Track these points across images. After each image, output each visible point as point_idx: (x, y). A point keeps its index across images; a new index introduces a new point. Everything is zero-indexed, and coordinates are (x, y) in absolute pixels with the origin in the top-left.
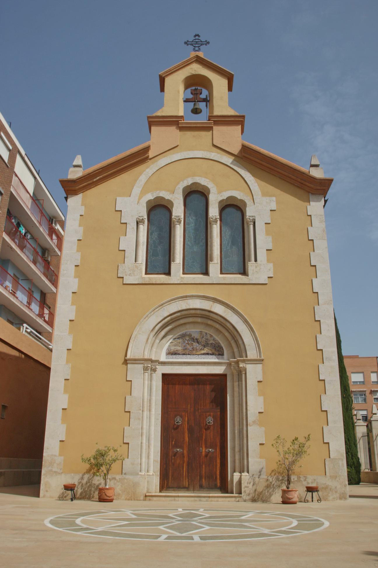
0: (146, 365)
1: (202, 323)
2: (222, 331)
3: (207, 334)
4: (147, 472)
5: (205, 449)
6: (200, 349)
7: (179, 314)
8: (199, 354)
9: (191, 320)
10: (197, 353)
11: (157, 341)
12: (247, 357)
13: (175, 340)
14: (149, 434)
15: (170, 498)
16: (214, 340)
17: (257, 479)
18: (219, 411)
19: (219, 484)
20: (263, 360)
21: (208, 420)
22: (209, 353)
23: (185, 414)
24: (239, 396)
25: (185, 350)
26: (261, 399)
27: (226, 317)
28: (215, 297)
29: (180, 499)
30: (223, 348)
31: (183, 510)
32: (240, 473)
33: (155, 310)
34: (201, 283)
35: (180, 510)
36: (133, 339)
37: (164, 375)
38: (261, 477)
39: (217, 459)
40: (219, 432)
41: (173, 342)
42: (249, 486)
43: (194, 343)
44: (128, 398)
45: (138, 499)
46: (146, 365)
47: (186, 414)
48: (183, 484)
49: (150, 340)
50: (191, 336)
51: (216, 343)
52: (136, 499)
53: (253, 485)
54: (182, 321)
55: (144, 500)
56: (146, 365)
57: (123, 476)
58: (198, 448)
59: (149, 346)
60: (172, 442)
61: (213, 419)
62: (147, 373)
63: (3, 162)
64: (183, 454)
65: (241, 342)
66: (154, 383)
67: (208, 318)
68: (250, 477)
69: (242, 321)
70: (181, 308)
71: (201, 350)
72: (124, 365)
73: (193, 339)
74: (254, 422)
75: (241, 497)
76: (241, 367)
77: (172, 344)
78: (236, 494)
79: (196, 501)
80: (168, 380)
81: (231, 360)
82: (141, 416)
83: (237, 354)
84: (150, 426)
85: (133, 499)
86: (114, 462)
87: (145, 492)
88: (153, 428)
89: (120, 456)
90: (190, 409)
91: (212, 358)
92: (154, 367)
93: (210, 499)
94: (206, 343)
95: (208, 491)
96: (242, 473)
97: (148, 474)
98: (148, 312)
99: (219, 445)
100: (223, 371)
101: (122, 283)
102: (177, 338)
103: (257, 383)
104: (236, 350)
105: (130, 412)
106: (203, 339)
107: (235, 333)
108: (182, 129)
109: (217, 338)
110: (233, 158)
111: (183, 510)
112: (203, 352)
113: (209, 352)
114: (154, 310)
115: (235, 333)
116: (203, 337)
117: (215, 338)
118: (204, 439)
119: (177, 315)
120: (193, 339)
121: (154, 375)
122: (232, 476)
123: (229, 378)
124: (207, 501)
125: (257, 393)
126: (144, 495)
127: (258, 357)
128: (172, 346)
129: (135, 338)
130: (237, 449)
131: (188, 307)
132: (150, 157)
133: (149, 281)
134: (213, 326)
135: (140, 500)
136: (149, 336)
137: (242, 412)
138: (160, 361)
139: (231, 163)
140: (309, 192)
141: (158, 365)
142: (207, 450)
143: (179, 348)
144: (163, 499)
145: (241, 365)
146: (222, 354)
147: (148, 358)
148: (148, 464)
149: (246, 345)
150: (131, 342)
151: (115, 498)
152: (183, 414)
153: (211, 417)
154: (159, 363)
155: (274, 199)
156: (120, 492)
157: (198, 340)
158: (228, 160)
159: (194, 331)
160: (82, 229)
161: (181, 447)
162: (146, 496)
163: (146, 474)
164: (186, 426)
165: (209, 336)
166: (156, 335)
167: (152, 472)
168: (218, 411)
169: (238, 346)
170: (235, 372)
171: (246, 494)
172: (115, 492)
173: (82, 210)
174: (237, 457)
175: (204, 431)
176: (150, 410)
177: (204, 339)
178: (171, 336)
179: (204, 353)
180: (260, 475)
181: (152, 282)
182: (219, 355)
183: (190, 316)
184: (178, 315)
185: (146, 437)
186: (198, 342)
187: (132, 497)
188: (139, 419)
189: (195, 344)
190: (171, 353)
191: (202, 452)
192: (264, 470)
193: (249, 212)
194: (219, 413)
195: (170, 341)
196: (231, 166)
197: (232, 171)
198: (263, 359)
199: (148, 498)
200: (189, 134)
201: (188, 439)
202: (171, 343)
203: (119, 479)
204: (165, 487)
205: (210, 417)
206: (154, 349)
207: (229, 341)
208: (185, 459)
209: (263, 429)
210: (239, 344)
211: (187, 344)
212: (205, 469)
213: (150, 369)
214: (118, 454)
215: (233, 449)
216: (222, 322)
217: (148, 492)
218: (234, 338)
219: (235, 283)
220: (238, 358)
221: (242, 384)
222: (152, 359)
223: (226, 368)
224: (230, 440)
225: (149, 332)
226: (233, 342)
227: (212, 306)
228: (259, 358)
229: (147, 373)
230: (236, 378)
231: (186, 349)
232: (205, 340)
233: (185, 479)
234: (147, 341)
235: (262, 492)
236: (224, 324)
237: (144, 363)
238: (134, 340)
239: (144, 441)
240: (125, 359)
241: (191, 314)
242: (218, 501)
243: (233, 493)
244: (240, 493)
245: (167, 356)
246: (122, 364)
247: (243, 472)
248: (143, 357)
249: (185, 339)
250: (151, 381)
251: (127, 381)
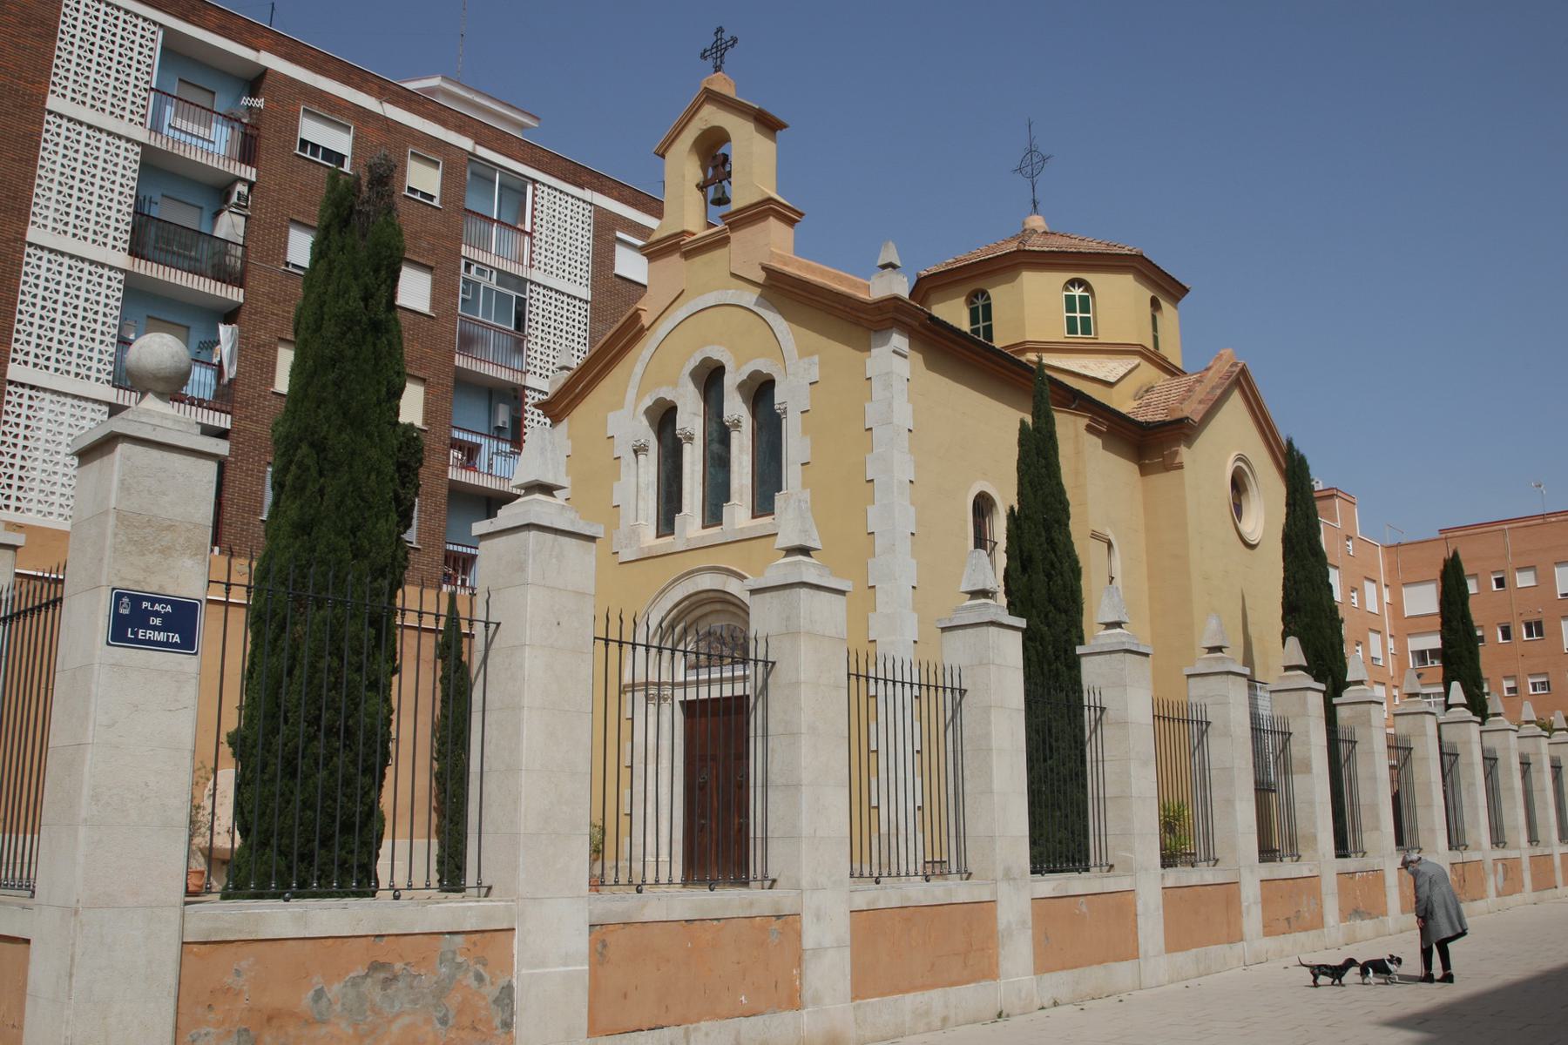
7: (686, 603)
9: (708, 608)
63: (636, 287)
108: (688, 255)
110: (759, 290)
131: (696, 590)
132: (646, 326)
140: (870, 329)
158: (749, 297)
196: (756, 309)
200: (699, 260)
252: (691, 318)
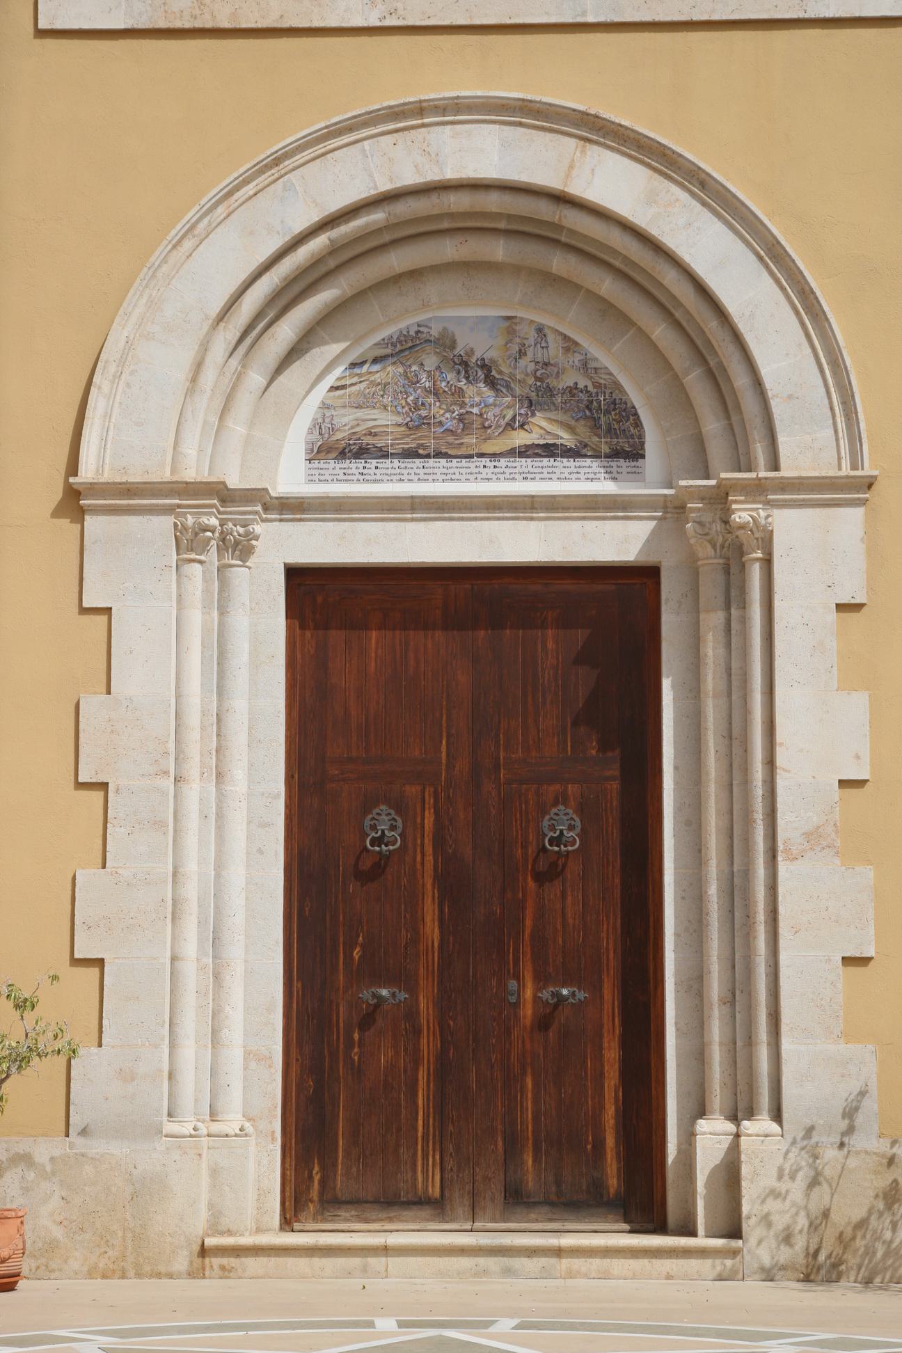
0: (190, 520)
1: (516, 270)
2: (634, 317)
3: (547, 331)
4: (208, 1118)
5: (538, 989)
6: (503, 423)
7: (377, 217)
8: (497, 450)
9: (449, 249)
10: (489, 448)
11: (256, 379)
12: (775, 466)
13: (357, 371)
14: (217, 907)
15: (340, 1262)
17: (831, 1154)
18: (617, 773)
19: (613, 1182)
20: (869, 484)
21: (553, 828)
22: (554, 445)
23: (424, 789)
24: (730, 694)
25: (417, 427)
26: (857, 705)
27: (654, 231)
28: (593, 112)
29: (394, 1262)
30: (640, 412)
31: (401, 1324)
32: (734, 1118)
33: (236, 196)
34: (509, 22)
35: (386, 1324)
36: (112, 369)
37: (297, 576)
38: (857, 1141)
39: (605, 1045)
40: (618, 893)
41: (348, 383)
42: (787, 1192)
43: (470, 391)
44: (93, 706)
45: (162, 1268)
46: (189, 517)
47: (429, 791)
48: (415, 1186)
49: (209, 376)
50: (453, 345)
51: (597, 385)
52: (147, 1269)
53: (814, 1183)
54: (397, 261)
55: (196, 1273)
56: (190, 520)
57: (72, 1146)
58: (494, 983)
59: (204, 406)
60: (352, 949)
61: (578, 823)
62: (201, 562)
64: (411, 1014)
65: (741, 380)
66: (240, 621)
67: (551, 237)
68: (794, 1142)
69: (753, 257)
70: (391, 180)
71: (510, 426)
72: (64, 523)
73: (465, 364)
74: (813, 837)
75: (735, 1253)
76: (742, 527)
77: (340, 397)
78: (709, 1235)
79: (485, 1272)
80: (320, 599)
81: (683, 483)
82: (171, 810)
83: (717, 450)
84: (219, 866)
85: (132, 1273)
86: (20, 1067)
87: (201, 1233)
88: (237, 875)
89: (50, 1035)
90: (450, 767)
91: (575, 476)
92: (241, 530)
93: (565, 1263)
94: (537, 389)
95: (551, 1220)
96: (745, 1123)
97: (216, 1128)
98: (197, 208)
99: (612, 964)
100: (639, 546)
101: (31, 30)
102: (371, 356)
103: (832, 616)
104: (712, 426)
105: (104, 786)
106: (523, 363)
107: (712, 325)
111: (401, 1324)
112: (520, 438)
113: (559, 442)
114: (230, 194)
115: (712, 325)
116: (522, 353)
117: (596, 360)
118: (528, 932)
119: (367, 225)
120: (463, 365)
121: (240, 576)
122: (689, 1137)
123: (670, 589)
124: (545, 1274)
125: (835, 670)
126: (196, 1248)
127: (840, 468)
128: (345, 407)
129: (122, 362)
130: (715, 988)
131: (432, 175)
133: (198, 12)
134: (578, 287)
135: (170, 1276)
136: (205, 347)
137: (746, 782)
138: (273, 494)
141: (263, 521)
142: (545, 995)
144: (302, 1263)
145: (742, 514)
146: (636, 454)
147: (205, 476)
148: (214, 1073)
149: (770, 394)
150: (99, 388)
151: (26, 1266)
152: (412, 790)
153: (570, 811)
154: (266, 508)
156: (58, 1233)
157: (494, 373)
161: (403, 978)
162: (204, 1252)
163: (205, 1132)
164: (429, 859)
165: (554, 349)
166: (248, 341)
167: (240, 1116)
168: (608, 773)
169: (727, 404)
170: (705, 551)
171: (772, 1233)
172: (28, 1235)
174: (716, 1031)
175: (531, 884)
176: (220, 776)
177: (526, 364)
178: (335, 348)
179: (528, 447)
180: (851, 1130)
181: (214, 17)
182: (616, 454)
183: (446, 225)
184: (375, 222)
185: (201, 923)
186: (491, 383)
187: (124, 1258)
188: (159, 825)
189: (477, 394)
191: (516, 1005)
192: (870, 1105)
194: (615, 786)
195: (330, 380)
198: (875, 477)
199: (216, 1261)
201: (437, 931)
202: (334, 388)
203: (52, 1159)
204: (311, 1201)
205: (562, 807)
206: (237, 427)
207: (676, 377)
208: (424, 1041)
209: (866, 874)
210: (733, 392)
211: (428, 391)
212: (536, 1101)
213: (213, 542)
214: (42, 1024)
215: (695, 984)
216: (635, 265)
217: (214, 1229)
218: (701, 353)
219: (716, 17)
220: (723, 475)
221: (745, 621)
222: (224, 483)
223: (653, 532)
224: (677, 935)
225: (206, 327)
226: (694, 380)
227: (571, 167)
228: (846, 470)
229: (197, 566)
230: (711, 588)
231: (426, 422)
232: (532, 367)
233: (425, 1157)
234: (194, 380)
235: (862, 1224)
236: (643, 270)
237: (179, 506)
238: (118, 376)
239: (190, 949)
240: (67, 483)
241: (451, 216)
242: (606, 1276)
243: (693, 1234)
244: (735, 1232)
245: (316, 464)
247: (751, 1113)
248: (172, 473)
249: (414, 368)
250: (223, 610)
251: (84, 611)
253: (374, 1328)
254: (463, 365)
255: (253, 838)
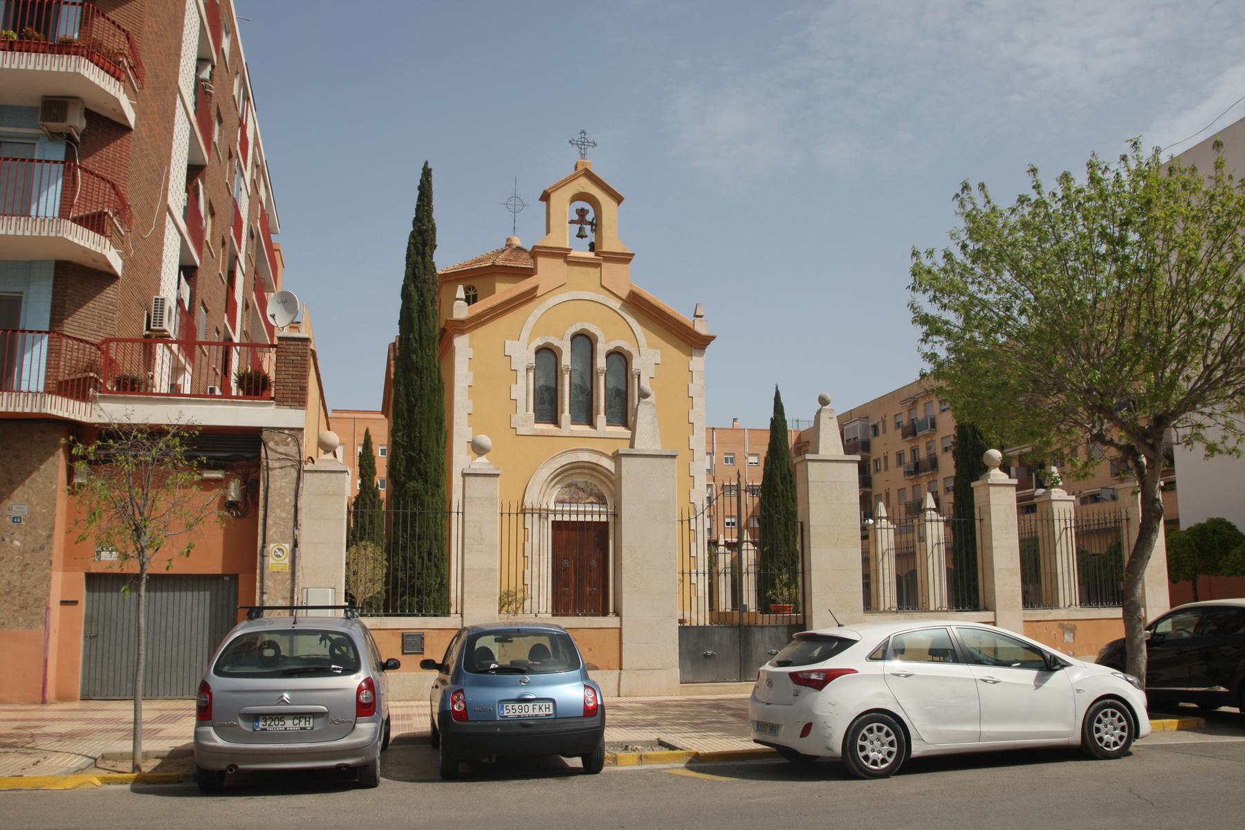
9: (578, 471)
16: (598, 490)
37: (554, 522)
54: (570, 472)
67: (594, 469)
109: (600, 488)
110: (621, 302)
120: (579, 489)
139: (620, 309)
143: (566, 497)
155: (659, 351)
158: (616, 304)
159: (580, 480)
160: (471, 374)
173: (469, 353)
189: (581, 493)
190: (557, 502)
193: (636, 365)
196: (620, 312)
197: (619, 317)
200: (577, 270)
246: (540, 200)
252: (612, 311)
253: (467, 720)
254: (579, 489)
255: (1062, 427)
